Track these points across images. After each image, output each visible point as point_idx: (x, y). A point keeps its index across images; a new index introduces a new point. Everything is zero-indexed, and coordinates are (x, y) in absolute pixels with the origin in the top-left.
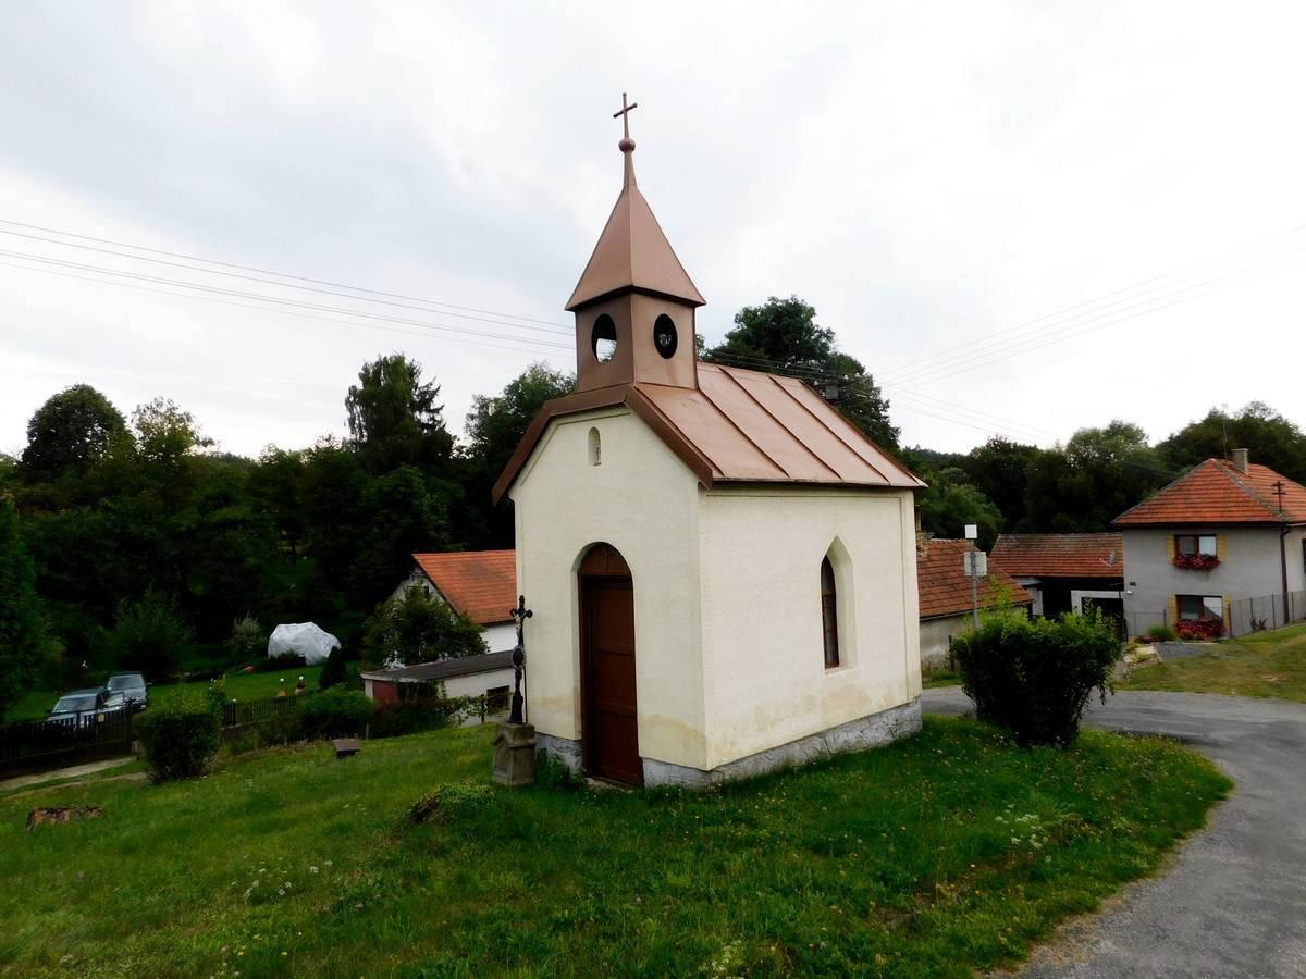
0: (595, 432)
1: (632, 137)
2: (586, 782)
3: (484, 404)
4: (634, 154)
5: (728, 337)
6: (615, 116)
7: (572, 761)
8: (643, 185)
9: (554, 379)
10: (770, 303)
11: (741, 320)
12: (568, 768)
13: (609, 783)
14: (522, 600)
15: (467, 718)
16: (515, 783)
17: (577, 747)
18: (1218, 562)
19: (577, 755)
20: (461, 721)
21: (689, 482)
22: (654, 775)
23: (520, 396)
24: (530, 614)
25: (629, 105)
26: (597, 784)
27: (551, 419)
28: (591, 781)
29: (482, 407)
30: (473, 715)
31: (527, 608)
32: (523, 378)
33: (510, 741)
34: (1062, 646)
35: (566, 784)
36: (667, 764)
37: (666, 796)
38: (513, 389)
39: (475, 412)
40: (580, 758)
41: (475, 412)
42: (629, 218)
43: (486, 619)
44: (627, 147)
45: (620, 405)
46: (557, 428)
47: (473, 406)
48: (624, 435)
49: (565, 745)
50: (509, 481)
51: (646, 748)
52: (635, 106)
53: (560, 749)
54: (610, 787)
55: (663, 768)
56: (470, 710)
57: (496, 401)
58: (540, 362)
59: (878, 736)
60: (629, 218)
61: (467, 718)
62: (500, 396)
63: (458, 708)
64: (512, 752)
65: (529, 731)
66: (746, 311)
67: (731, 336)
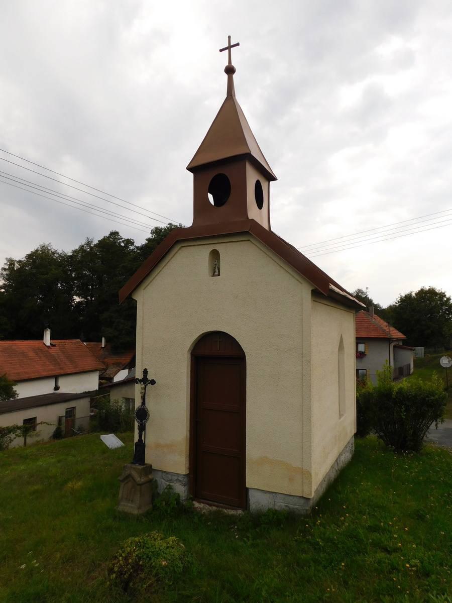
0: (215, 255)
1: (233, 64)
2: (193, 505)
3: (11, 262)
4: (235, 76)
5: (146, 240)
6: (221, 51)
7: (181, 490)
8: (240, 98)
9: (53, 253)
10: (169, 226)
11: (154, 233)
12: (179, 494)
13: (210, 505)
14: (145, 372)
15: (15, 438)
16: (141, 512)
17: (186, 479)
18: (366, 355)
19: (185, 485)
20: (11, 441)
21: (304, 291)
22: (258, 501)
23: (34, 261)
24: (153, 382)
25: (232, 44)
26: (202, 505)
27: (178, 242)
28: (197, 505)
29: (11, 264)
30: (19, 436)
31: (150, 377)
32: (37, 251)
33: (138, 479)
34: (427, 399)
35: (181, 511)
36: (272, 492)
37: (284, 520)
38: (30, 257)
39: (7, 267)
40: (186, 487)
41: (7, 267)
42: (229, 119)
43: (15, 378)
44: (230, 71)
45: (246, 233)
46: (180, 249)
47: (6, 264)
48: (239, 257)
49: (175, 478)
50: (133, 288)
51: (251, 480)
52: (238, 44)
53: (171, 481)
54: (214, 508)
55: (268, 495)
56: (17, 433)
57: (20, 262)
58: (47, 243)
59: (347, 457)
60: (229, 119)
61: (15, 438)
62: (23, 260)
63: (10, 432)
64: (138, 487)
65: (149, 469)
66: (156, 228)
67: (148, 240)
